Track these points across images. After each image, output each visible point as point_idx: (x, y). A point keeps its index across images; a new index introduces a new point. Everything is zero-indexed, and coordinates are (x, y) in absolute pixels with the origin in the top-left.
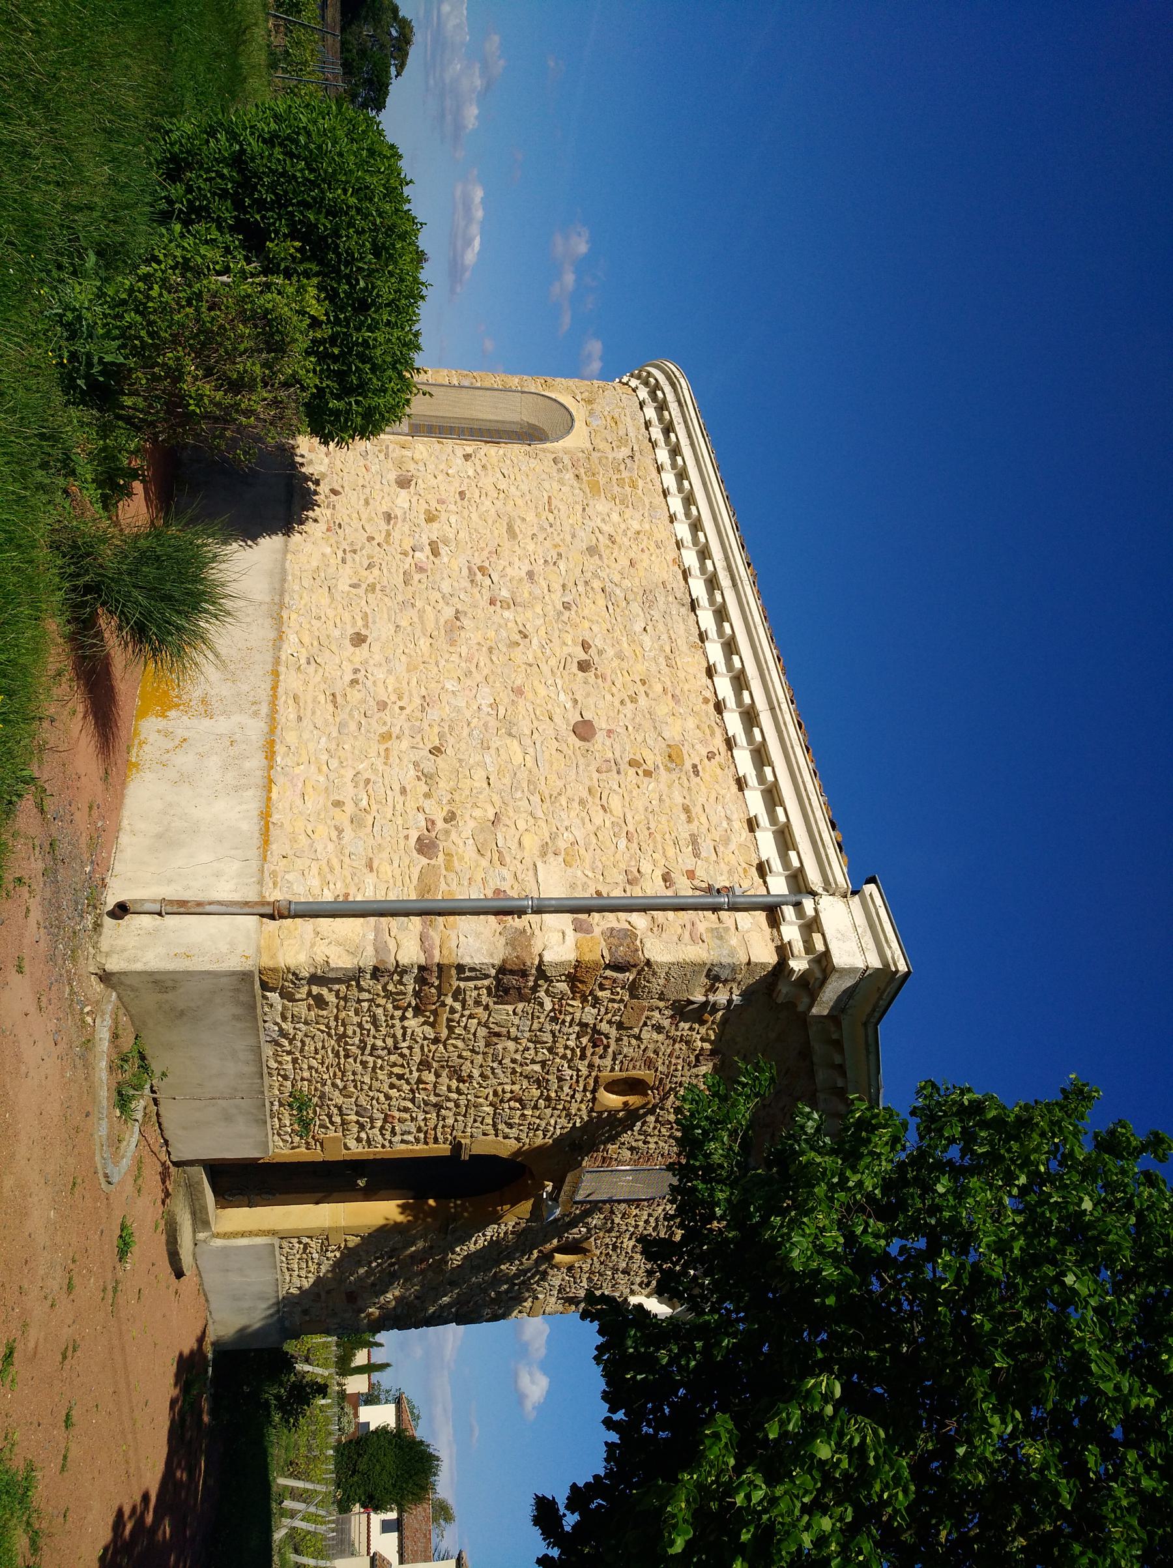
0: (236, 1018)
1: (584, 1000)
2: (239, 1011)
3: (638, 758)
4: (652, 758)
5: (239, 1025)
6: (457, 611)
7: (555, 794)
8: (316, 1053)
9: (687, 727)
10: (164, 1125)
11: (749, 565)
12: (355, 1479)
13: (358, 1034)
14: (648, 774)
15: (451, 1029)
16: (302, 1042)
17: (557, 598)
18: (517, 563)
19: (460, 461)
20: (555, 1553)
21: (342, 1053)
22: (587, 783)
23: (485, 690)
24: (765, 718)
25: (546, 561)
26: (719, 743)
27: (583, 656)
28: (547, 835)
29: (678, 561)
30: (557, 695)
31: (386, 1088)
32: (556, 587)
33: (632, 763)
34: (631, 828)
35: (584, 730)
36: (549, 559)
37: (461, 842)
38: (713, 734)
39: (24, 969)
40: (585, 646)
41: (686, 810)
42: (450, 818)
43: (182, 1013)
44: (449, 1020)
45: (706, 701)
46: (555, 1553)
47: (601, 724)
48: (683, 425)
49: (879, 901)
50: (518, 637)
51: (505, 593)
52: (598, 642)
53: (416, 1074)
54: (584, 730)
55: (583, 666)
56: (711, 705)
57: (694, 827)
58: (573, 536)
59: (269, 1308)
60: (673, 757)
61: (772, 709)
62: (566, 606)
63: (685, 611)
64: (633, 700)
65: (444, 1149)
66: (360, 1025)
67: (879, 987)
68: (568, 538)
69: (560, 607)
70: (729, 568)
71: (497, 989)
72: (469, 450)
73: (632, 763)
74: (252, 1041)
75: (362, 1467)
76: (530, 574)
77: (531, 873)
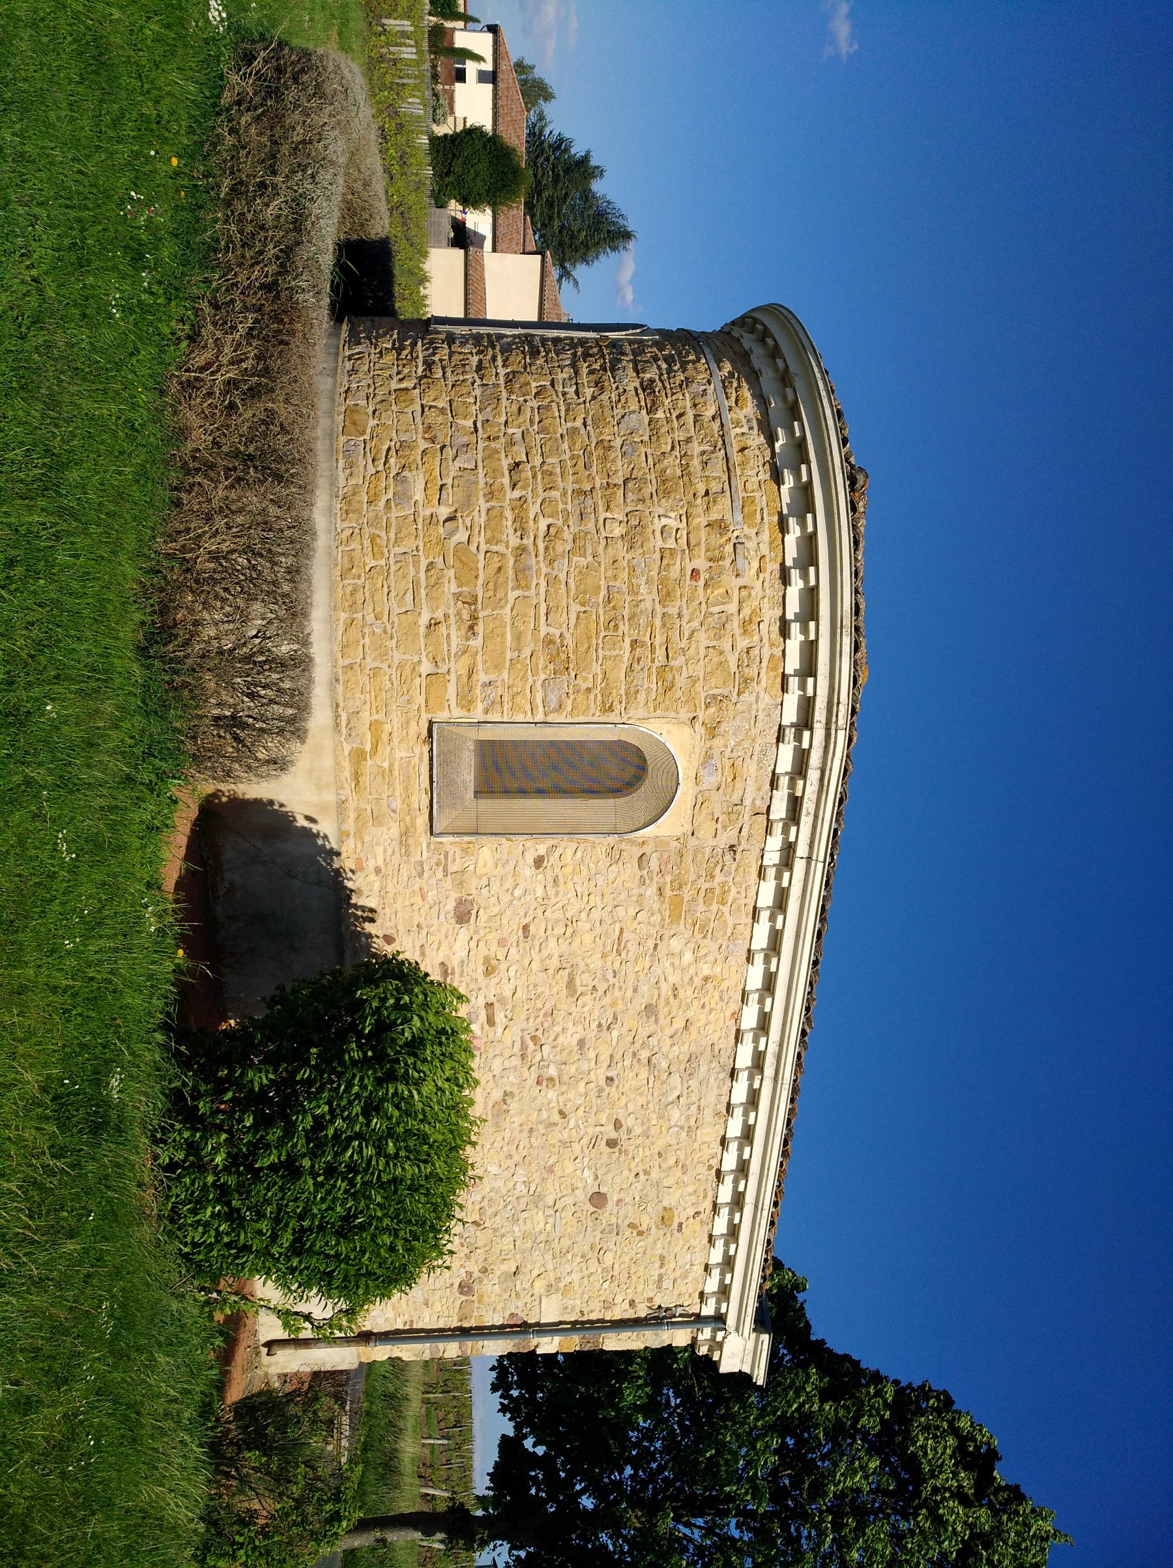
3: (636, 1222)
4: (646, 1221)
6: (506, 1094)
7: (564, 1251)
9: (683, 1196)
11: (772, 1223)
12: (451, 179)
14: (640, 1233)
17: (601, 1074)
18: (572, 1029)
19: (528, 871)
22: (592, 1240)
23: (520, 1171)
24: (748, 1210)
25: (600, 1025)
26: (708, 1205)
27: (613, 1135)
28: (552, 1279)
29: (737, 1017)
30: (580, 1174)
32: (604, 1058)
33: (631, 1226)
34: (616, 1273)
35: (598, 1199)
36: (603, 1022)
37: (491, 1288)
38: (705, 1197)
40: (617, 1125)
41: (662, 1258)
42: (484, 1270)
45: (710, 1167)
47: (613, 1198)
48: (811, 817)
49: (766, 1346)
50: (556, 1117)
51: (552, 1071)
52: (629, 1122)
54: (598, 1199)
55: (612, 1143)
56: (713, 1172)
57: (663, 1271)
58: (635, 990)
60: (665, 1219)
61: (756, 1206)
62: (610, 1080)
63: (724, 1075)
64: (646, 1173)
67: (742, 1380)
68: (629, 993)
69: (602, 1082)
70: (779, 1058)
72: (542, 850)
73: (631, 1226)
75: (457, 169)
76: (581, 1043)
77: (537, 1302)
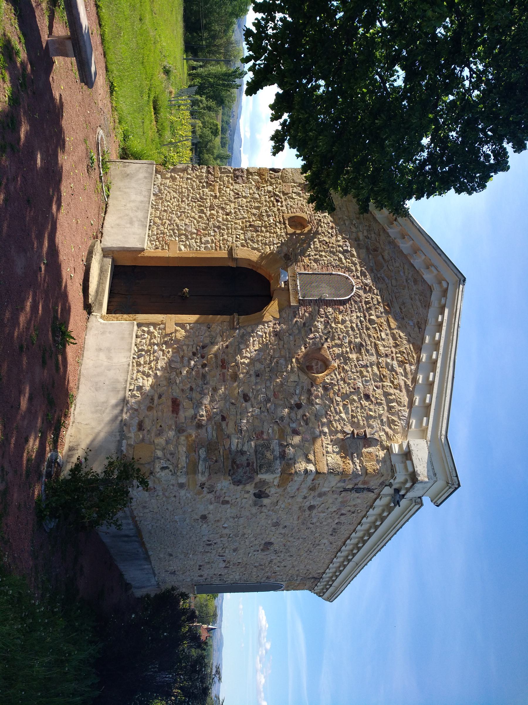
0: (145, 178)
1: (213, 54)
2: (146, 175)
5: (146, 180)
8: (171, 199)
10: (105, 224)
13: (186, 192)
15: (220, 192)
16: (166, 195)
20: (508, 147)
21: (180, 200)
31: (197, 217)
39: (170, 403)
43: (128, 175)
44: (219, 189)
46: (508, 147)
53: (209, 212)
59: (66, 286)
65: (224, 254)
66: (187, 188)
71: (235, 177)
74: (148, 187)
